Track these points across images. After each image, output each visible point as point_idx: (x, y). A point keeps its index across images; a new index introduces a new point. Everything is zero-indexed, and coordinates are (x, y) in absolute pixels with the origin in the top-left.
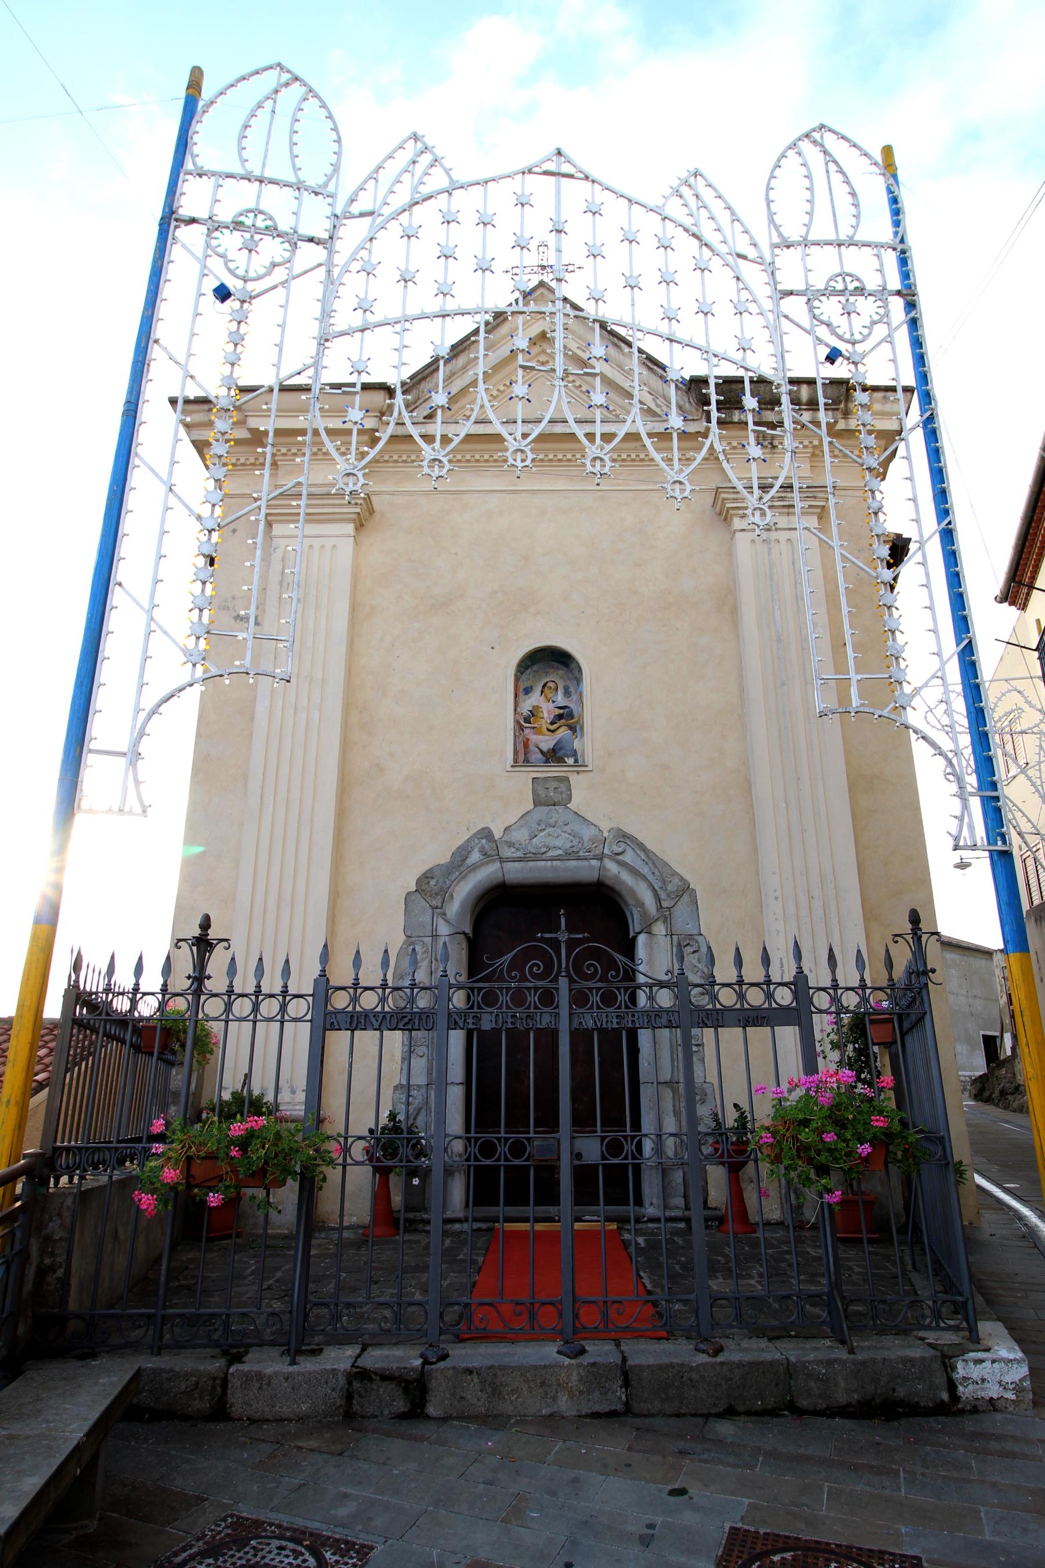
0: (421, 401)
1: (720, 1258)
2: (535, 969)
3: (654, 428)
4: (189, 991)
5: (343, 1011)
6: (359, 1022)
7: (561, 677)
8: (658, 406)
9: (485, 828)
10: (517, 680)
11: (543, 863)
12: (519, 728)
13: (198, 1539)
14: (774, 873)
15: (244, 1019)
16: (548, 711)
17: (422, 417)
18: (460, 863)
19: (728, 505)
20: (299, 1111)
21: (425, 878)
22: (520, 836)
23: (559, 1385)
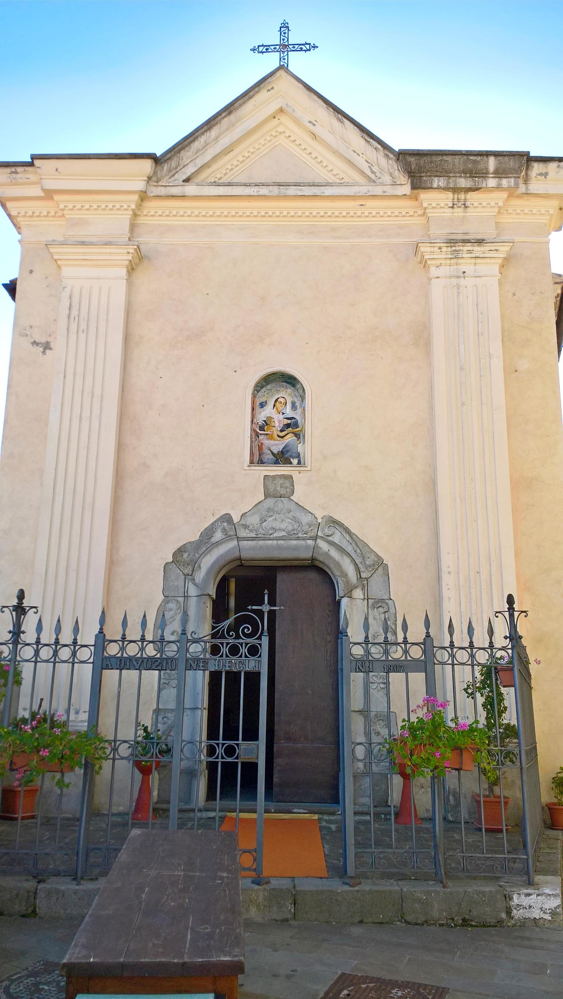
0: (181, 167)
1: (387, 839)
2: (246, 630)
3: (369, 191)
4: (10, 642)
5: (114, 657)
6: (125, 664)
7: (289, 395)
8: (373, 172)
9: (227, 514)
10: (254, 396)
11: (270, 542)
12: (255, 435)
13: (24, 970)
14: (449, 553)
15: (47, 661)
16: (278, 421)
17: (181, 180)
18: (207, 541)
19: (426, 257)
20: (84, 727)
21: (180, 551)
22: (253, 520)
23: (251, 901)
